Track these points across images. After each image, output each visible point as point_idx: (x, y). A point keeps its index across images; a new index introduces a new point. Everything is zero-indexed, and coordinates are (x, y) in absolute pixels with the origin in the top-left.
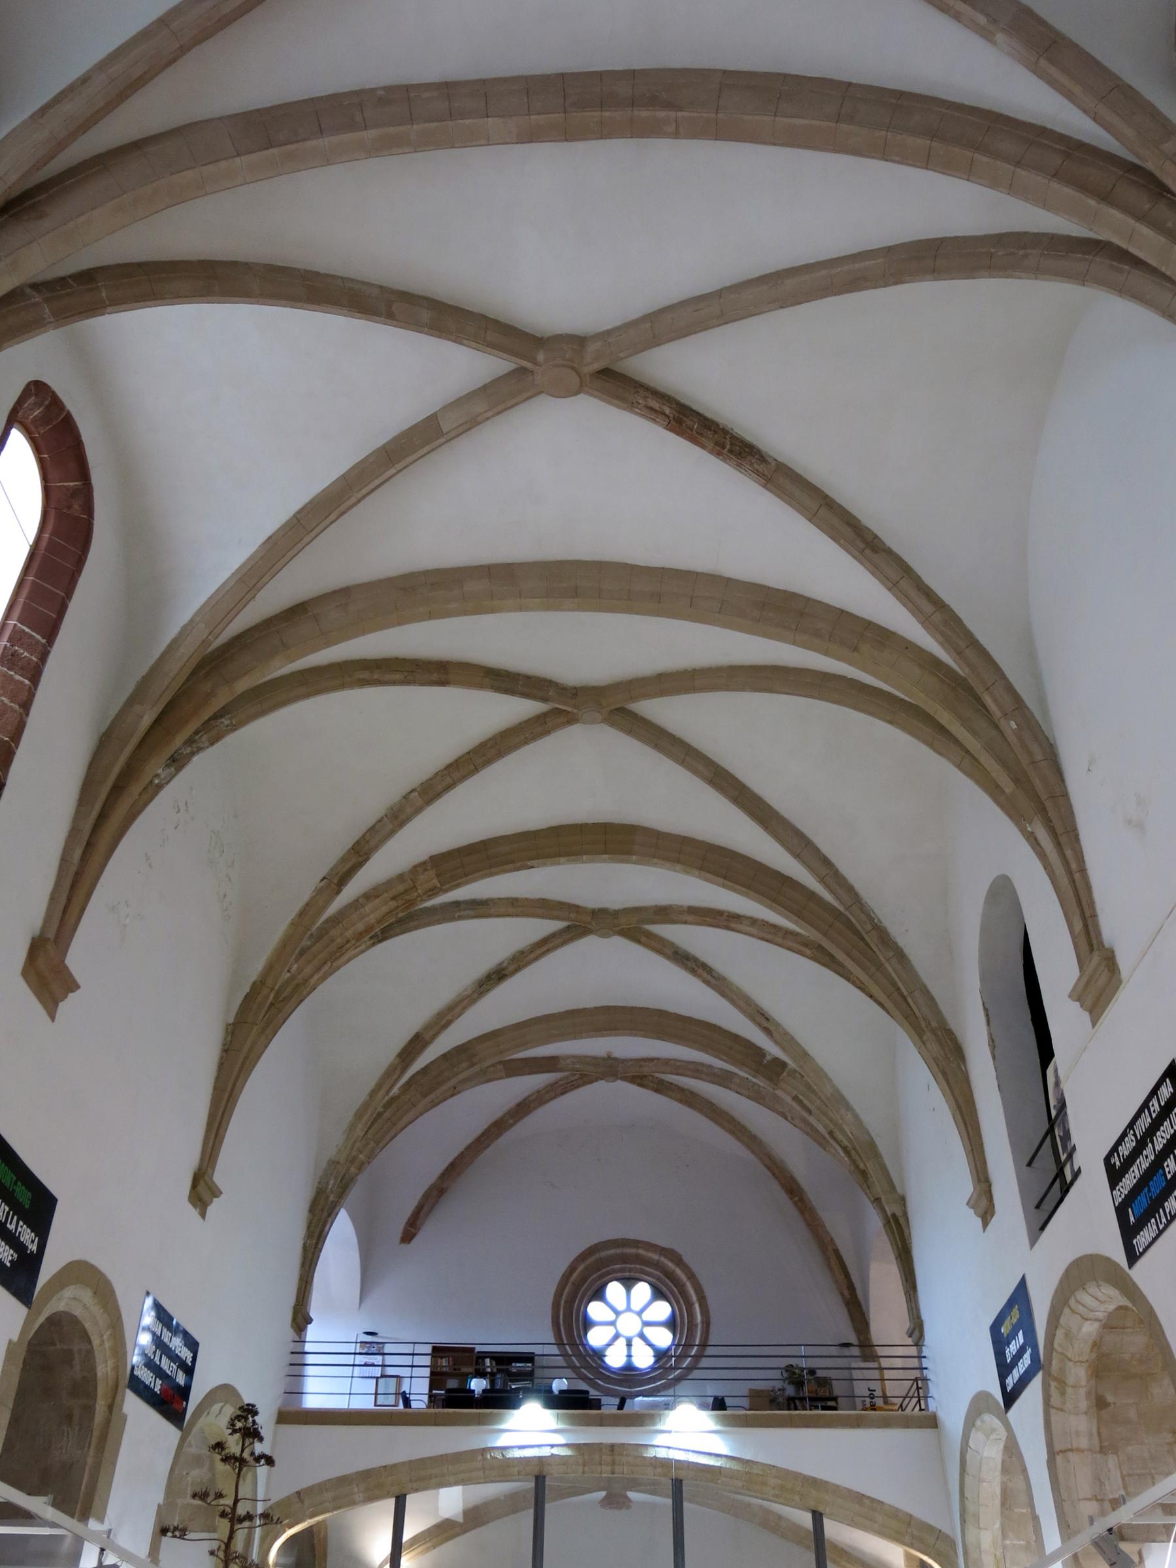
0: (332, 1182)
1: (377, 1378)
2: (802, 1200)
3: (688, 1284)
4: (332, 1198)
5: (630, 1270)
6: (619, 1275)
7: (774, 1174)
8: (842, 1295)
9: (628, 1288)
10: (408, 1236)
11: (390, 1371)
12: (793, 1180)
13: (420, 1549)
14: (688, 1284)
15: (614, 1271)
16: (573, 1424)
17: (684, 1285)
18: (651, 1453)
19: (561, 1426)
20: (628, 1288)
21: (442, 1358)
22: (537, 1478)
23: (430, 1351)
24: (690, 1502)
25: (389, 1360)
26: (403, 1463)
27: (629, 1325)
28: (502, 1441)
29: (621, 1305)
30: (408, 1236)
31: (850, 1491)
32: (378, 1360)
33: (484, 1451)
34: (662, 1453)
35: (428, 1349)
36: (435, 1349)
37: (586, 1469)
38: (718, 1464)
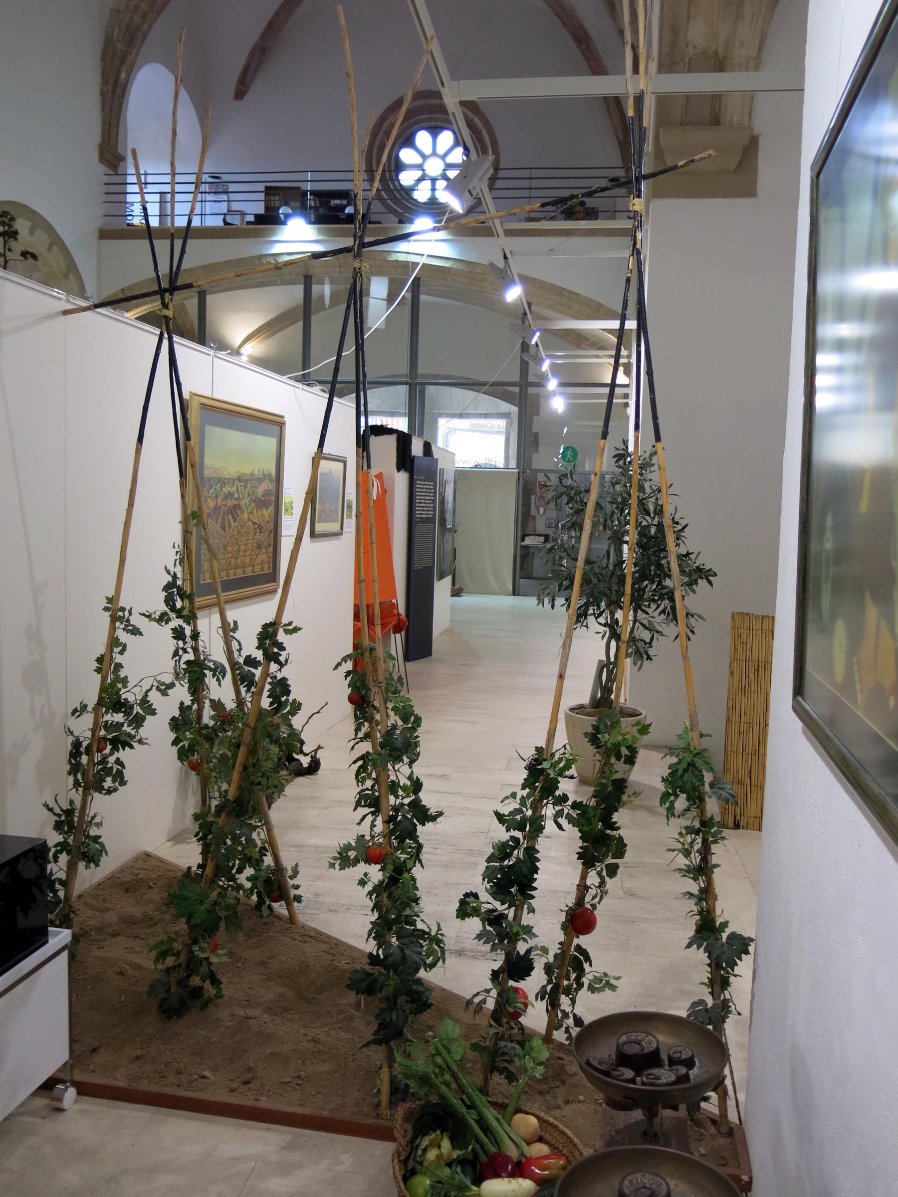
0: (116, 30)
1: (225, 214)
2: (588, 48)
3: (484, 130)
4: (119, 46)
5: (436, 120)
6: (424, 124)
7: (563, 23)
8: (617, 137)
9: (435, 136)
10: (240, 94)
11: (236, 206)
12: (581, 28)
13: (264, 336)
14: (484, 130)
15: (421, 121)
16: (331, 236)
17: (481, 131)
18: (394, 257)
19: (321, 238)
20: (435, 136)
21: (274, 196)
22: (305, 277)
23: (263, 189)
24: (427, 294)
25: (233, 197)
26: (199, 268)
27: (434, 167)
28: (277, 249)
29: (427, 150)
30: (240, 94)
31: (553, 285)
32: (224, 197)
33: (261, 257)
34: (402, 258)
35: (261, 187)
36: (267, 188)
37: (342, 270)
38: (447, 265)
